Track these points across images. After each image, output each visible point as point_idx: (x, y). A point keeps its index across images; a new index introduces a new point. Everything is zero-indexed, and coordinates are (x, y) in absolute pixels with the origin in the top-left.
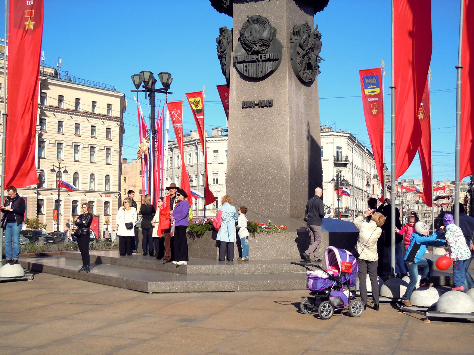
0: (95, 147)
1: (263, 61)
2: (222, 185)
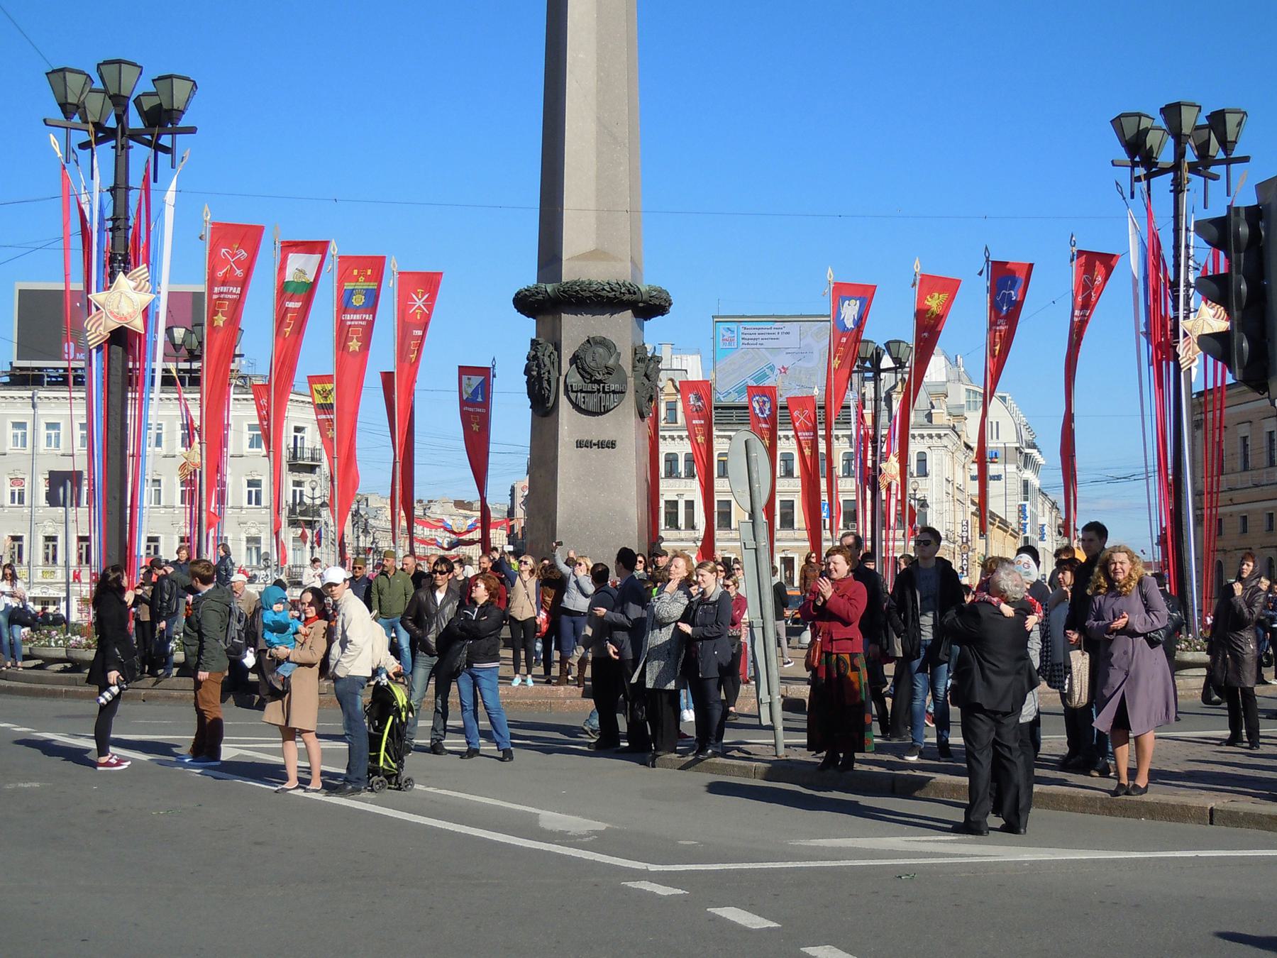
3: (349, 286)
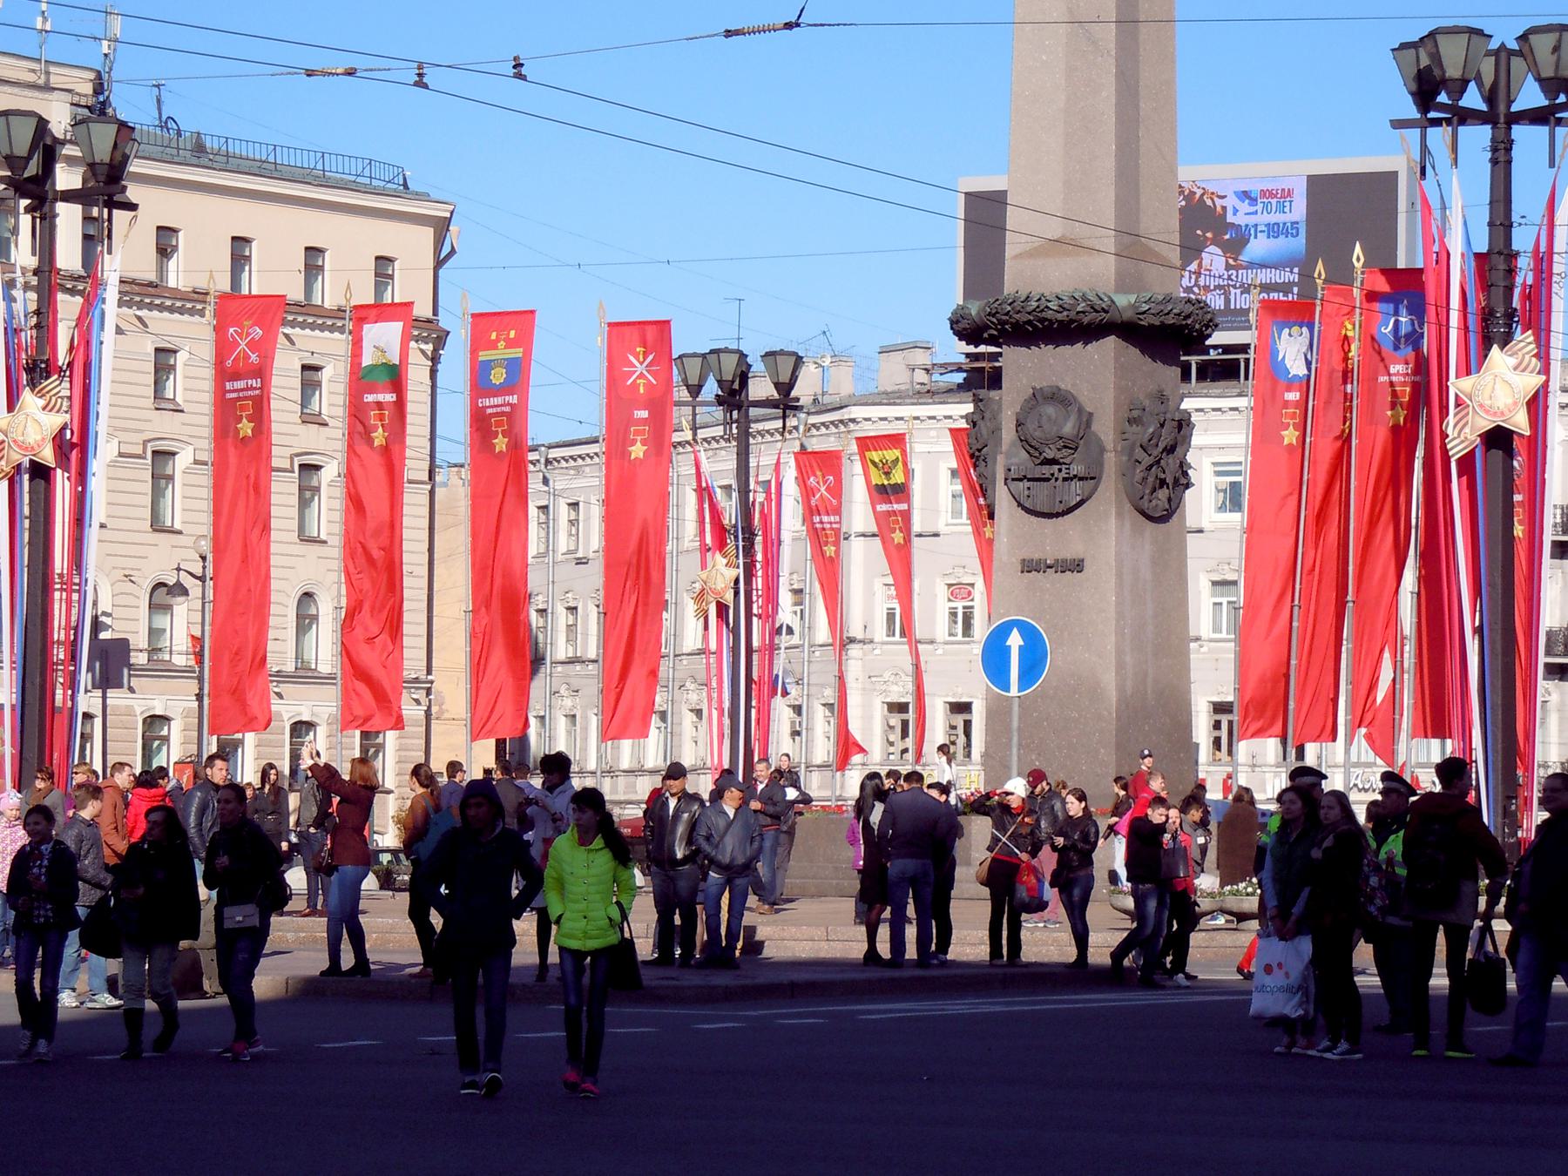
0: (317, 468)
1: (1065, 479)
2: (932, 642)
3: (484, 356)
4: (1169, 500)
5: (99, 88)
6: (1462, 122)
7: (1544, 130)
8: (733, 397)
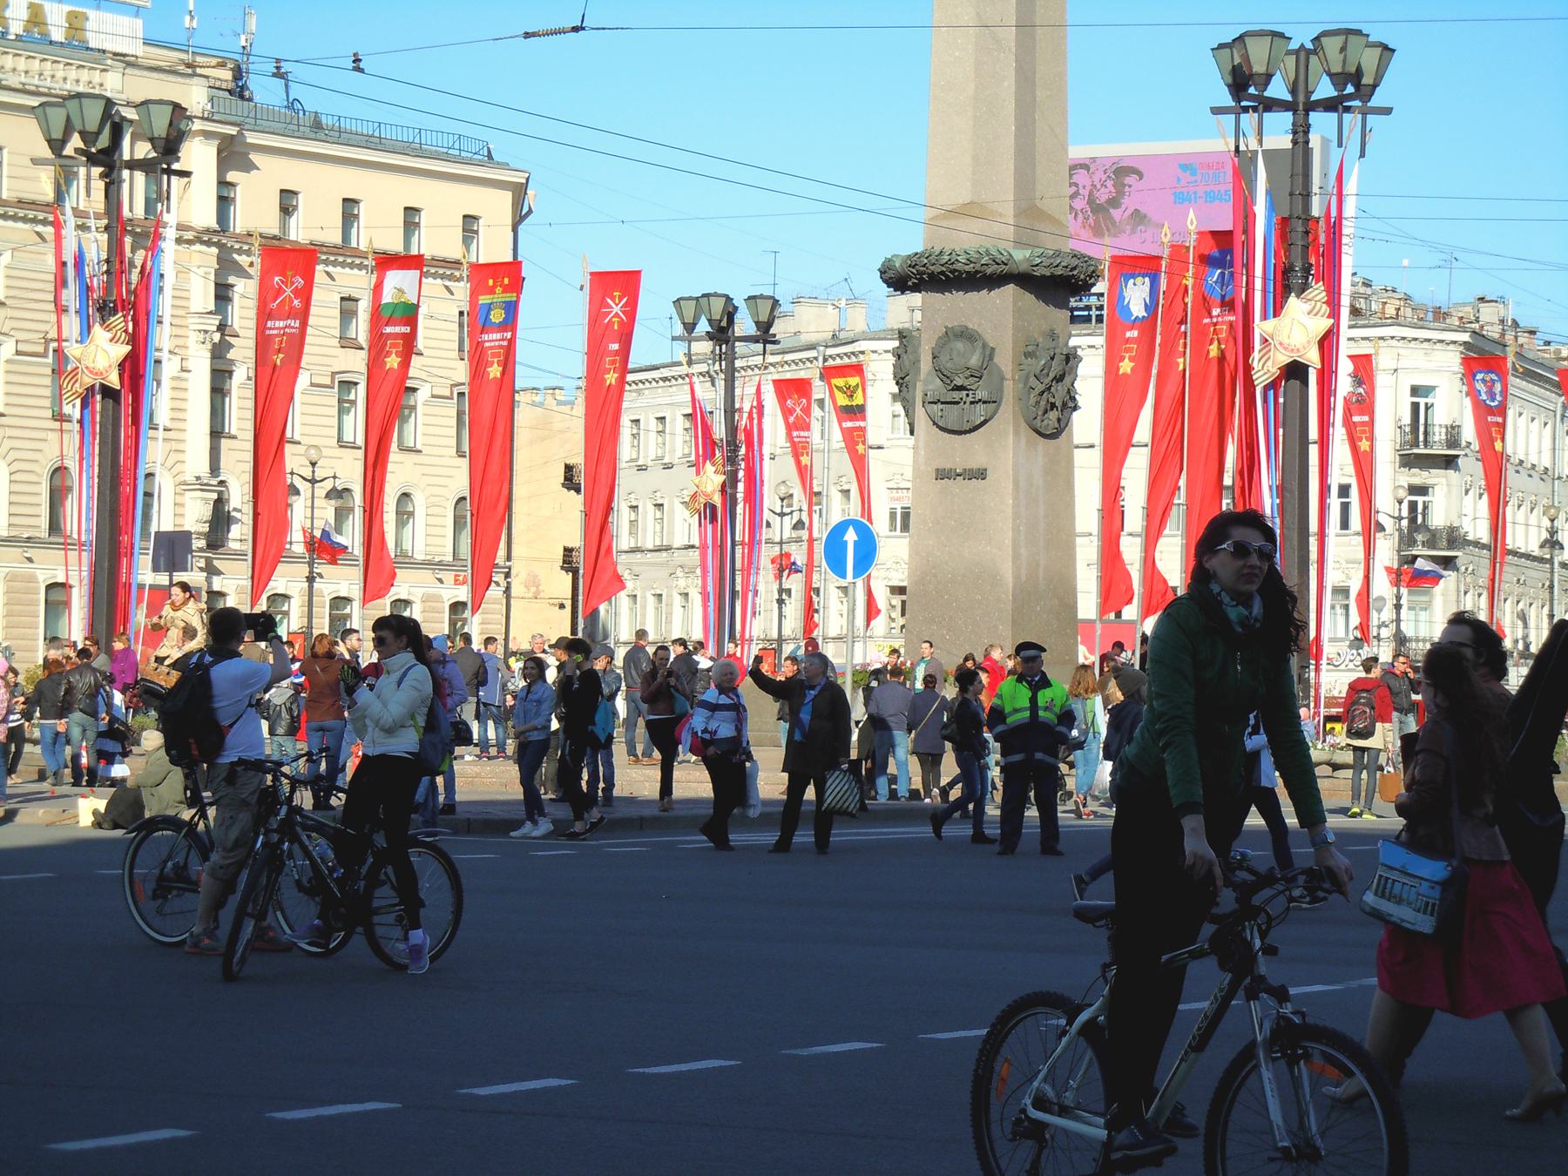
0: (414, 390)
3: (484, 300)
4: (1059, 420)
5: (238, 73)
6: (1268, 109)
7: (1335, 116)
8: (722, 333)
